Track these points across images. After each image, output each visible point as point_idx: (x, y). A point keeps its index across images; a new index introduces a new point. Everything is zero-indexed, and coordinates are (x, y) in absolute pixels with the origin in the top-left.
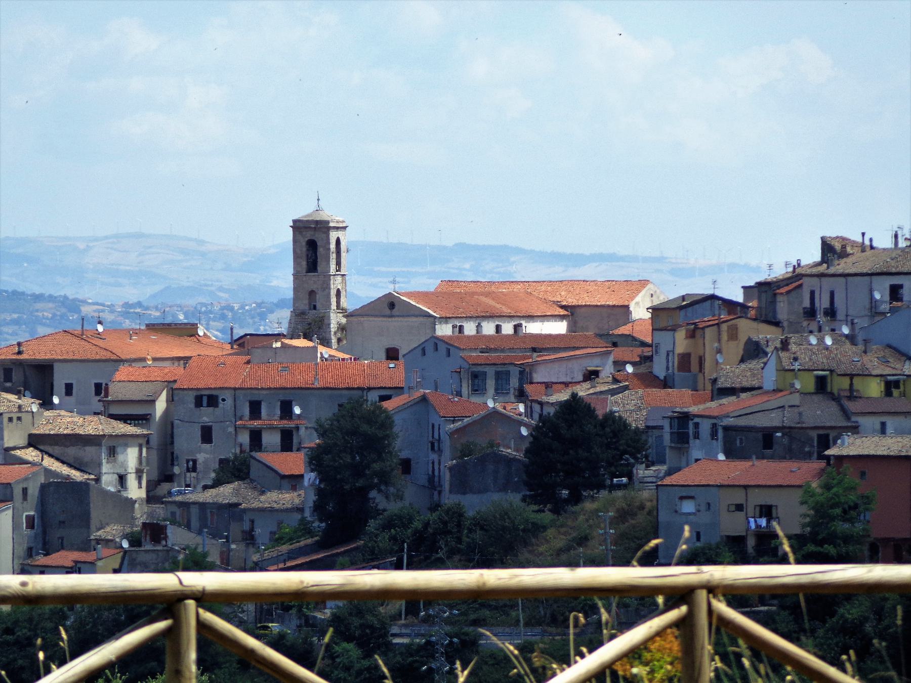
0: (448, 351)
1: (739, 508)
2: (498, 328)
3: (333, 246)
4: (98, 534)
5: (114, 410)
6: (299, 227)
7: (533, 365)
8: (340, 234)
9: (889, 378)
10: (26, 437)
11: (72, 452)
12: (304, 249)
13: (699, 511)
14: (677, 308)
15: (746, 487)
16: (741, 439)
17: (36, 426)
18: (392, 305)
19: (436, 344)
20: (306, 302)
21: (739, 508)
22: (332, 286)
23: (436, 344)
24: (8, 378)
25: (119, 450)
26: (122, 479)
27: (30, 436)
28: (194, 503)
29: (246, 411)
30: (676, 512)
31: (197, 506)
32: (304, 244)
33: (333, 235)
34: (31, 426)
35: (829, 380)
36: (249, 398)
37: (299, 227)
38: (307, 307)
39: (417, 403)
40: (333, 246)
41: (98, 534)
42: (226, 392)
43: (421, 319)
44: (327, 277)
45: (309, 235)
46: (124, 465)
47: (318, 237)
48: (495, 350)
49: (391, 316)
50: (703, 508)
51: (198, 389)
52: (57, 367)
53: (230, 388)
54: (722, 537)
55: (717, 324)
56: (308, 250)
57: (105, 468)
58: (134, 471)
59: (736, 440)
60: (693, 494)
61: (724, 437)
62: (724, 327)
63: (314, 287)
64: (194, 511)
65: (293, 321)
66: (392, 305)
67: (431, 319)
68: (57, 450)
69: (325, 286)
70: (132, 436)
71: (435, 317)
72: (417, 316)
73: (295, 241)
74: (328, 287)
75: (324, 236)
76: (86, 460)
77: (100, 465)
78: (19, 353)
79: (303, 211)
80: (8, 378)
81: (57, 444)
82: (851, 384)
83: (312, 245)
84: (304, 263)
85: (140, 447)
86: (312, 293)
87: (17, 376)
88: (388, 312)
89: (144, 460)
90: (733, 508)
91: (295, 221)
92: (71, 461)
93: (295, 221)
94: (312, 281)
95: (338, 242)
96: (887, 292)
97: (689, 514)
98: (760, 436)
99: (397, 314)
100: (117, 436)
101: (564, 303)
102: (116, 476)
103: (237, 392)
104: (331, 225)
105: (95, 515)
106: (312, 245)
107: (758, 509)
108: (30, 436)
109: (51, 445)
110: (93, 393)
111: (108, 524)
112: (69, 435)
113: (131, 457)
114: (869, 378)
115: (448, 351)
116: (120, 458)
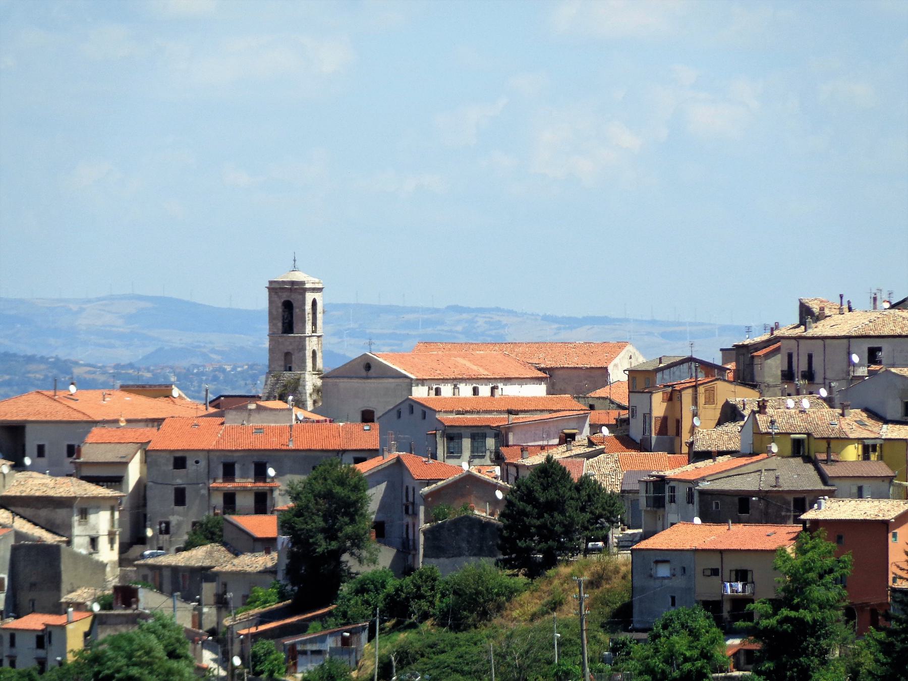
2: (475, 391)
3: (308, 307)
6: (275, 289)
8: (317, 296)
11: (44, 513)
12: (280, 310)
13: (674, 575)
15: (721, 552)
16: (717, 504)
17: (7, 487)
20: (282, 363)
22: (308, 348)
26: (94, 541)
30: (651, 576)
32: (280, 305)
33: (309, 297)
37: (275, 289)
40: (308, 307)
45: (285, 296)
47: (294, 298)
49: (367, 378)
50: (679, 571)
53: (203, 450)
56: (284, 311)
60: (668, 558)
61: (701, 501)
63: (290, 348)
66: (368, 367)
67: (407, 380)
68: (28, 512)
71: (412, 379)
72: (393, 378)
73: (271, 302)
74: (303, 348)
75: (300, 297)
76: (58, 521)
83: (288, 306)
84: (280, 325)
86: (288, 355)
88: (364, 373)
90: (709, 573)
91: (271, 282)
95: (314, 303)
96: (866, 355)
98: (736, 500)
99: (374, 375)
101: (543, 366)
102: (87, 539)
103: (212, 453)
104: (307, 286)
106: (288, 306)
107: (733, 574)
111: (79, 587)
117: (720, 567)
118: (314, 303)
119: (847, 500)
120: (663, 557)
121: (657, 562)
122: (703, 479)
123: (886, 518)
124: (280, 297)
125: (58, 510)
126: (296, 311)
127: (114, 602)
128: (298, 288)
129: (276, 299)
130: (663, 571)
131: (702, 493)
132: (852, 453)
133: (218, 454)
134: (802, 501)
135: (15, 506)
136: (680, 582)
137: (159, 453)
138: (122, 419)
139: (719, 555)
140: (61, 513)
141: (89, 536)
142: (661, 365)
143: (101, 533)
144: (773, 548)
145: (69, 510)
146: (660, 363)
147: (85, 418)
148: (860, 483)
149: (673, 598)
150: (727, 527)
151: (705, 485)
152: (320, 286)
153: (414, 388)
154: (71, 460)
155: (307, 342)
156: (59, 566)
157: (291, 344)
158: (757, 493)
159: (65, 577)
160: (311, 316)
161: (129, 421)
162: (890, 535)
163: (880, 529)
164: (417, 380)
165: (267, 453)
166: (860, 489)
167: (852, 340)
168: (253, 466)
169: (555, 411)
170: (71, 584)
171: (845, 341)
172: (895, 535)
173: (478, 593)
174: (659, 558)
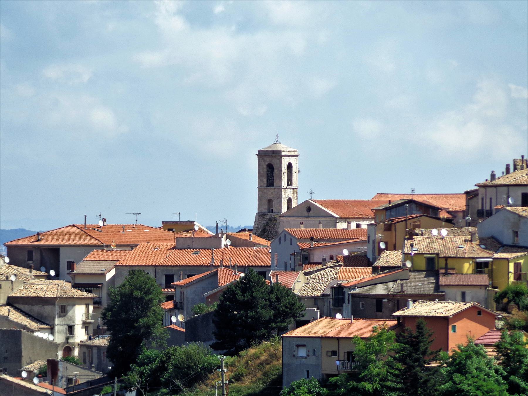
0: (291, 239)
1: (334, 353)
2: (358, 226)
3: (284, 168)
4: (27, 367)
5: (79, 280)
6: (262, 155)
7: (311, 250)
8: (292, 160)
9: (478, 260)
10: (6, 298)
11: (36, 309)
12: (265, 170)
13: (308, 356)
14: (384, 209)
15: (338, 339)
16: (363, 304)
17: (15, 290)
18: (309, 209)
19: (285, 235)
20: (266, 207)
21: (334, 353)
22: (283, 196)
23: (285, 235)
24: (30, 258)
25: (68, 308)
26: (71, 329)
27: (9, 298)
28: (95, 346)
29: (163, 281)
30: (294, 356)
31: (96, 348)
32: (265, 167)
33: (285, 162)
34: (10, 290)
35: (436, 261)
36: (165, 273)
37: (262, 155)
38: (266, 211)
39: (208, 278)
40: (284, 168)
41: (27, 367)
42: (150, 268)
43: (328, 219)
44: (280, 189)
45: (268, 160)
46: (72, 319)
47: (274, 162)
48: (323, 240)
49: (308, 217)
50: (311, 353)
51: (130, 266)
52: (62, 250)
53: (151, 266)
54: (323, 374)
55: (405, 220)
56: (268, 171)
57: (57, 321)
58: (81, 322)
59: (359, 304)
60: (305, 343)
61: (353, 301)
62: (408, 222)
63: (271, 197)
64: (95, 351)
65: (257, 221)
66: (309, 209)
67: (334, 219)
68: (26, 308)
69: (278, 196)
70: (79, 298)
71: (336, 218)
72: (324, 217)
73: (259, 165)
74: (280, 197)
75: (278, 161)
76: (45, 314)
77: (54, 318)
78: (39, 240)
79: (265, 146)
80: (30, 258)
81: (26, 304)
82: (446, 264)
83: (270, 167)
84: (265, 180)
85: (87, 306)
86: (270, 201)
87: (36, 256)
88: (306, 214)
89: (90, 315)
90: (330, 354)
91: (259, 151)
92: (36, 316)
93: (259, 151)
94: (270, 192)
95: (290, 166)
96: (520, 198)
97: (303, 357)
98: (374, 301)
99: (312, 215)
100: (66, 298)
101: (450, 210)
102: (66, 327)
103: (157, 268)
104: (283, 153)
105: (25, 353)
106: (270, 167)
107: (346, 354)
108: (9, 298)
109: (23, 304)
110: (66, 268)
111: (36, 360)
112: (35, 297)
113: (79, 313)
114: (462, 260)
115: (291, 239)
116: (70, 314)
117: (338, 351)
118: (290, 166)
119: (428, 302)
120: (302, 342)
121: (298, 346)
122: (355, 286)
123: (447, 315)
124: (265, 161)
125: (45, 307)
126: (276, 171)
127: (48, 371)
128: (277, 155)
129: (263, 163)
130: (302, 352)
131: (354, 296)
132: (467, 267)
133: (162, 268)
134: (400, 301)
135: (18, 303)
136: (312, 361)
137: (123, 268)
138: (113, 244)
139: (337, 342)
140: (47, 309)
141: (67, 325)
142: (391, 205)
143: (76, 322)
144: (352, 336)
145: (52, 306)
146: (390, 203)
147: (99, 244)
148: (463, 290)
149: (308, 372)
150: (349, 321)
151: (357, 291)
152: (296, 154)
153: (337, 224)
154: (68, 272)
155: (283, 193)
156: (20, 346)
157: (272, 193)
158: (387, 296)
159: (24, 353)
160: (286, 175)
161: (118, 246)
162: (450, 327)
163: (443, 322)
164: (341, 218)
165: (195, 268)
166: (463, 294)
167: (511, 188)
168: (164, 277)
169: (354, 239)
170: (30, 358)
171: (506, 188)
172: (454, 328)
173: (189, 367)
174: (299, 343)
